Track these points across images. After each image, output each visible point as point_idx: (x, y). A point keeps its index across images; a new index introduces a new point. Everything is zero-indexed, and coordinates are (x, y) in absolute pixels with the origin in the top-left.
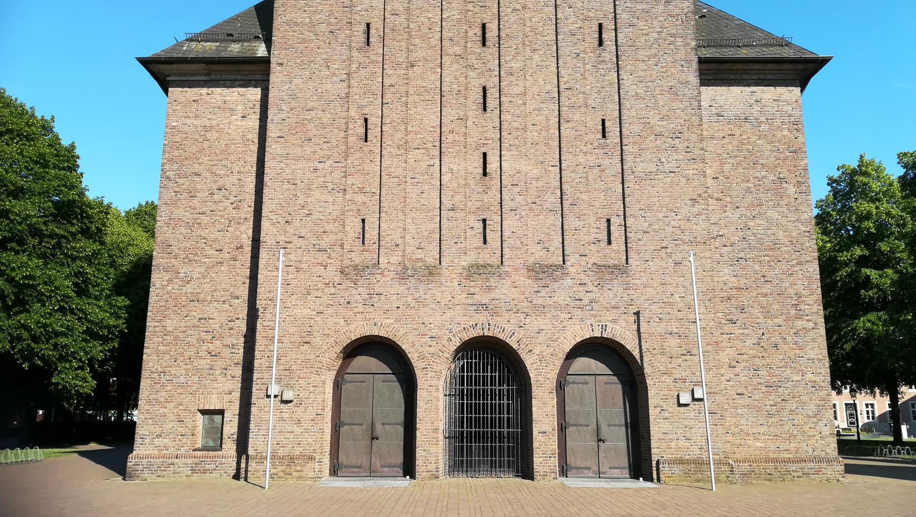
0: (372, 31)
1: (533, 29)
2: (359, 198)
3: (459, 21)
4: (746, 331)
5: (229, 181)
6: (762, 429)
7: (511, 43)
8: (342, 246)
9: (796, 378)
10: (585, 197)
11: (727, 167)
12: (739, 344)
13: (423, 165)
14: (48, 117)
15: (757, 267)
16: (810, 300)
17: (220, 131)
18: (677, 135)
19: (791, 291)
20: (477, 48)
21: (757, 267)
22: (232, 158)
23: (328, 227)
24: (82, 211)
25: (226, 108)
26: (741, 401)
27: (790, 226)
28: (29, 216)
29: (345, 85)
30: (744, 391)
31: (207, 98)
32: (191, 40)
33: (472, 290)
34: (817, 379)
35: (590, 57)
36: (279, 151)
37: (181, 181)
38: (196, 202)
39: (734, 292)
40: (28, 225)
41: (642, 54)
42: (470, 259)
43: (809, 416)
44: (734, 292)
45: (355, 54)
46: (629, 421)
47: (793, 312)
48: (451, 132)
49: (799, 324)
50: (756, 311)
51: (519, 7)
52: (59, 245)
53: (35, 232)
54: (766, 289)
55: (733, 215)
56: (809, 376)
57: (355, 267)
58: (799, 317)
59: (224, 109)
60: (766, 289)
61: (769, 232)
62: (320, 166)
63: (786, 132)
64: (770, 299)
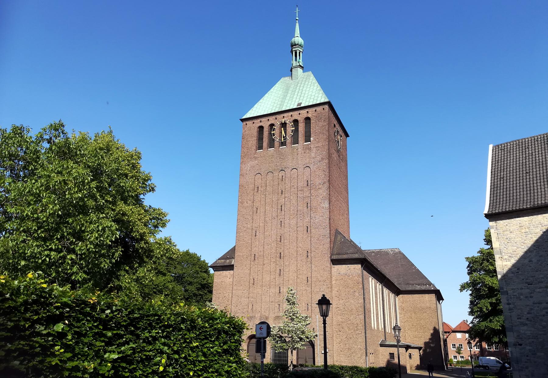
0: (256, 256)
1: (292, 254)
2: (252, 299)
3: (275, 253)
4: (343, 334)
5: (226, 295)
6: (346, 361)
7: (286, 258)
8: (248, 312)
9: (355, 347)
10: (302, 298)
11: (341, 288)
12: (341, 337)
13: (266, 290)
14: (199, 256)
15: (347, 316)
16: (361, 325)
17: (225, 282)
18: (325, 281)
19: (355, 323)
20: (278, 259)
21: (347, 316)
22: (227, 289)
23: (245, 307)
24: (208, 285)
25: (226, 276)
26: (342, 353)
27: (356, 305)
28: (193, 291)
29: (249, 271)
30: (342, 350)
31: (222, 274)
32: (219, 259)
33: (276, 323)
34: (361, 347)
35: (305, 260)
36: (235, 288)
37: (217, 295)
38: (220, 300)
39: (341, 323)
40: (193, 294)
41: (317, 259)
42: (276, 315)
43: (358, 358)
44: (341, 323)
45: (252, 262)
46: (445, 367)
47: (356, 329)
48: (272, 282)
49: (357, 332)
50: (346, 328)
51: (288, 248)
52: (202, 298)
53: (195, 295)
54: (349, 322)
55: (341, 302)
56: (359, 346)
57: (250, 317)
58: (357, 330)
59: (226, 277)
60: (349, 322)
61: (351, 306)
62: (243, 292)
63: (356, 278)
64: (350, 325)
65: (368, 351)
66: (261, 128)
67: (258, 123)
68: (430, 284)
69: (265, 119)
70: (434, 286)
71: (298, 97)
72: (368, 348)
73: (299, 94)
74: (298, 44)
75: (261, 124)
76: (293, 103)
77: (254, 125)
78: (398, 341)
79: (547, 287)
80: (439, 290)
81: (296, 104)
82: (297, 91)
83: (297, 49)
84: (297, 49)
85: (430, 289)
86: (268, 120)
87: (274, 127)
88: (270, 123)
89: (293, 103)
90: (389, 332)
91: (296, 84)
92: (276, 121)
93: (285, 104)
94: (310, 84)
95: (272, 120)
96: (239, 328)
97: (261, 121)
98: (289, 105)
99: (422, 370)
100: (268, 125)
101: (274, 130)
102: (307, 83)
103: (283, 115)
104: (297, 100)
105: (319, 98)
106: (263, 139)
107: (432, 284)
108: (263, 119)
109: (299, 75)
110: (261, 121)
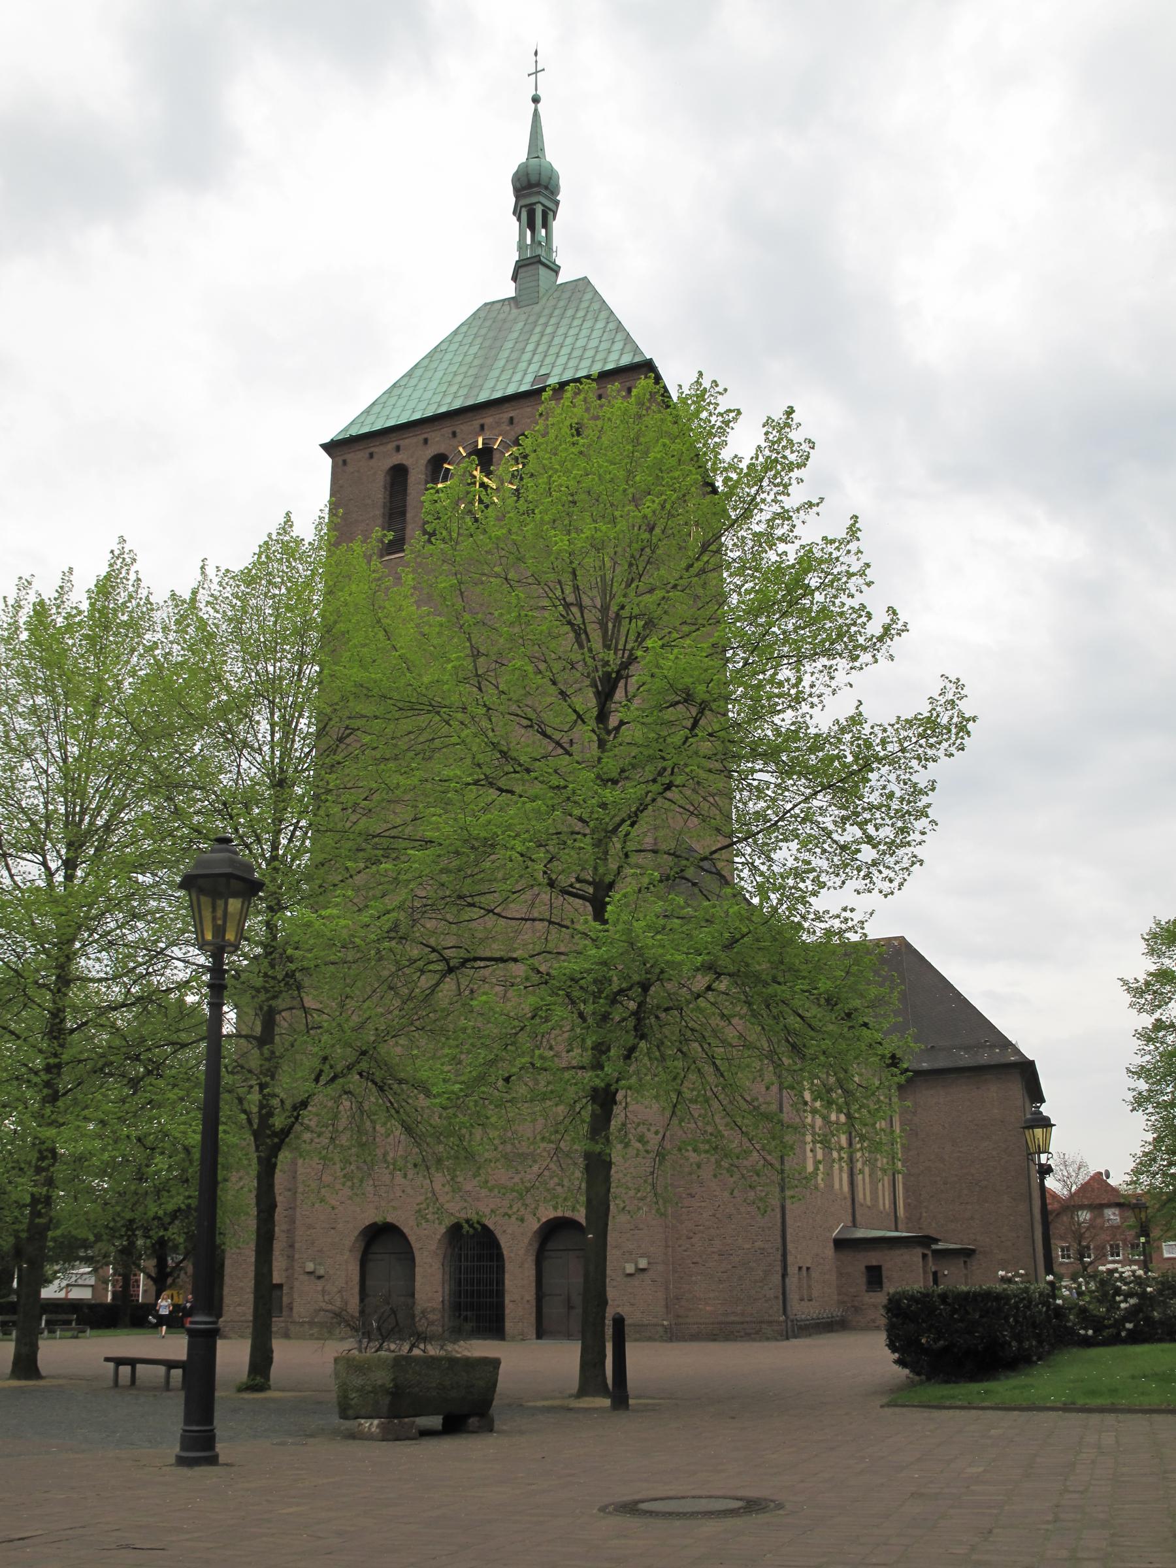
56: (759, 1244)
65: (790, 1259)
66: (399, 474)
67: (387, 458)
68: (1006, 1044)
69: (414, 440)
70: (1017, 1051)
71: (537, 358)
72: (790, 1246)
73: (541, 349)
74: (538, 184)
75: (397, 459)
76: (517, 377)
77: (373, 462)
78: (576, 722)
79: (1172, 1104)
80: (1032, 1063)
81: (529, 378)
82: (534, 338)
83: (533, 200)
84: (533, 200)
85: (1003, 1060)
86: (426, 441)
87: (446, 466)
88: (430, 452)
89: (517, 377)
90: (869, 1203)
91: (532, 319)
92: (454, 442)
93: (490, 384)
94: (581, 314)
95: (439, 442)
96: (1101, 1173)
97: (398, 449)
98: (501, 385)
99: (334, 506)
100: (423, 462)
101: (445, 479)
102: (570, 313)
103: (482, 421)
104: (533, 368)
105: (614, 356)
106: (403, 513)
107: (1010, 1043)
108: (410, 441)
109: (542, 291)
110: (398, 449)
